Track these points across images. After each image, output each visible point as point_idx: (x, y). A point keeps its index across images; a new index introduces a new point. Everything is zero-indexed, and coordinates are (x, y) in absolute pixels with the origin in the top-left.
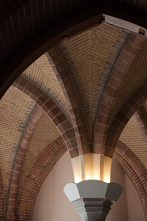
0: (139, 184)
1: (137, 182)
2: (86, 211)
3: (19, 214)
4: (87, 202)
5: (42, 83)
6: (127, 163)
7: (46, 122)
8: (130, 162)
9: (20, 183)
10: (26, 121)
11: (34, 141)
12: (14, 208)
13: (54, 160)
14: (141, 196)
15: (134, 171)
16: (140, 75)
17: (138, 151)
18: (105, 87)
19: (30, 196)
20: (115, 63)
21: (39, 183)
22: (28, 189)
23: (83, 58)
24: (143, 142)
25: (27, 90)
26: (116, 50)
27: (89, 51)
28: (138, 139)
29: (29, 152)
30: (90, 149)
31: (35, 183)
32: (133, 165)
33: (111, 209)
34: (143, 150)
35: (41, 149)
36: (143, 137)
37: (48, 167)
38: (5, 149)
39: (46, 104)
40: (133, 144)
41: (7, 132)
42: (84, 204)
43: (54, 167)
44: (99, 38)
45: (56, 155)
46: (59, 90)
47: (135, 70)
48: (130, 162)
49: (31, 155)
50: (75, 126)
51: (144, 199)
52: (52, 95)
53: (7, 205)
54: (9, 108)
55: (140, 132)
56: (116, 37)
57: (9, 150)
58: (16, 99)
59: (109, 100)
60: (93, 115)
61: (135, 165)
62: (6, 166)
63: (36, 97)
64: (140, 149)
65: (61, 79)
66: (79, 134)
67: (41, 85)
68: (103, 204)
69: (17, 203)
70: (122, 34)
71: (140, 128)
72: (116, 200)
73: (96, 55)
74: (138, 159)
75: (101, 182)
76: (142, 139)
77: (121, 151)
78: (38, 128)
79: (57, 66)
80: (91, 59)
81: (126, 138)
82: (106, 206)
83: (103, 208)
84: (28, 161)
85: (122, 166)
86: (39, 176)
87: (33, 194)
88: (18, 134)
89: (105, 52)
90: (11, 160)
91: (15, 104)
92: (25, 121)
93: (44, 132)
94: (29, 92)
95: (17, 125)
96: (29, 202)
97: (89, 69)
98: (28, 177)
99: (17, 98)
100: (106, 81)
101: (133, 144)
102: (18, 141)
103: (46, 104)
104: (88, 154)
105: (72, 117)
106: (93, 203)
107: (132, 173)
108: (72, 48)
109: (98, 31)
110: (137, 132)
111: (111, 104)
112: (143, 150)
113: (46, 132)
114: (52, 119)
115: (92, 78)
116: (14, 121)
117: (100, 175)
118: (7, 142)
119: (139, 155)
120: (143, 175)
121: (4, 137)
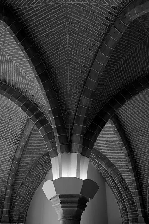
0: (116, 190)
1: (115, 188)
2: (62, 208)
3: (13, 217)
4: (62, 199)
5: (26, 91)
6: (107, 172)
7: (38, 136)
8: (109, 171)
9: (14, 189)
10: (20, 135)
11: (27, 153)
12: (8, 211)
13: (45, 170)
14: (118, 201)
15: (113, 179)
16: (115, 83)
17: (116, 162)
18: (82, 90)
19: (24, 201)
20: (91, 66)
21: (32, 189)
22: (21, 194)
23: (62, 62)
24: (120, 154)
25: (13, 98)
26: (92, 54)
27: (67, 56)
28: (116, 151)
29: (24, 162)
30: (69, 150)
31: (28, 190)
32: (112, 174)
33: (86, 206)
34: (121, 160)
35: (34, 160)
36: (121, 149)
37: (40, 176)
38: (3, 159)
39: (29, 110)
40: (112, 155)
41: (4, 144)
42: (60, 201)
43: (46, 176)
44: (76, 42)
45: (47, 166)
46: (41, 95)
47: (111, 76)
48: (109, 171)
49: (25, 165)
50: (54, 126)
51: (121, 203)
52: (35, 101)
53: (3, 208)
54: (6, 123)
55: (118, 145)
56: (92, 41)
57: (5, 160)
58: (11, 115)
59: (86, 101)
60: (71, 117)
61: (114, 174)
62: (3, 174)
63: (22, 104)
64: (118, 160)
65: (40, 81)
66: (57, 134)
67: (26, 93)
68: (79, 200)
69: (12, 206)
70: (98, 37)
71: (117, 141)
72: (92, 198)
73: (74, 59)
74: (116, 168)
75: (77, 179)
76: (119, 151)
77: (102, 162)
78: (31, 141)
79: (36, 68)
80: (69, 63)
81: (106, 151)
82: (82, 203)
83: (78, 205)
84: (22, 170)
85: (103, 175)
86: (32, 184)
87: (26, 199)
88: (14, 146)
89: (83, 56)
90: (7, 169)
91: (11, 120)
92: (19, 134)
93: (37, 145)
94: (15, 99)
95: (12, 138)
96: (22, 206)
97: (67, 73)
98: (22, 184)
99: (12, 113)
100: (84, 84)
101: (112, 155)
102: (14, 152)
103: (29, 110)
104: (66, 153)
105: (51, 118)
106: (69, 199)
107: (111, 181)
108: (51, 52)
109: (75, 35)
110: (115, 144)
111: (88, 104)
112: (121, 160)
113: (38, 145)
114: (35, 123)
115: (70, 82)
116: (10, 134)
117: (77, 173)
118: (4, 153)
119: (117, 165)
120: (120, 182)
121: (2, 149)
